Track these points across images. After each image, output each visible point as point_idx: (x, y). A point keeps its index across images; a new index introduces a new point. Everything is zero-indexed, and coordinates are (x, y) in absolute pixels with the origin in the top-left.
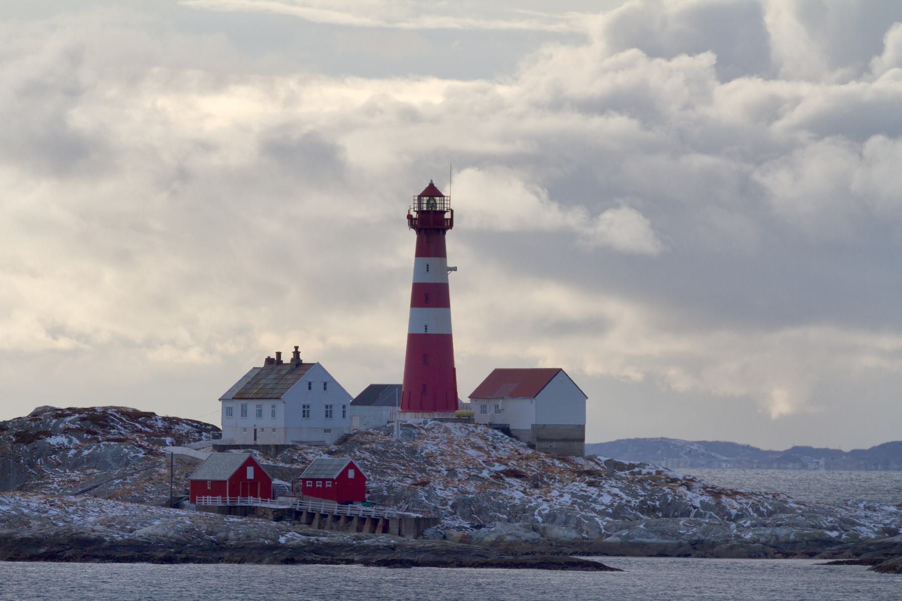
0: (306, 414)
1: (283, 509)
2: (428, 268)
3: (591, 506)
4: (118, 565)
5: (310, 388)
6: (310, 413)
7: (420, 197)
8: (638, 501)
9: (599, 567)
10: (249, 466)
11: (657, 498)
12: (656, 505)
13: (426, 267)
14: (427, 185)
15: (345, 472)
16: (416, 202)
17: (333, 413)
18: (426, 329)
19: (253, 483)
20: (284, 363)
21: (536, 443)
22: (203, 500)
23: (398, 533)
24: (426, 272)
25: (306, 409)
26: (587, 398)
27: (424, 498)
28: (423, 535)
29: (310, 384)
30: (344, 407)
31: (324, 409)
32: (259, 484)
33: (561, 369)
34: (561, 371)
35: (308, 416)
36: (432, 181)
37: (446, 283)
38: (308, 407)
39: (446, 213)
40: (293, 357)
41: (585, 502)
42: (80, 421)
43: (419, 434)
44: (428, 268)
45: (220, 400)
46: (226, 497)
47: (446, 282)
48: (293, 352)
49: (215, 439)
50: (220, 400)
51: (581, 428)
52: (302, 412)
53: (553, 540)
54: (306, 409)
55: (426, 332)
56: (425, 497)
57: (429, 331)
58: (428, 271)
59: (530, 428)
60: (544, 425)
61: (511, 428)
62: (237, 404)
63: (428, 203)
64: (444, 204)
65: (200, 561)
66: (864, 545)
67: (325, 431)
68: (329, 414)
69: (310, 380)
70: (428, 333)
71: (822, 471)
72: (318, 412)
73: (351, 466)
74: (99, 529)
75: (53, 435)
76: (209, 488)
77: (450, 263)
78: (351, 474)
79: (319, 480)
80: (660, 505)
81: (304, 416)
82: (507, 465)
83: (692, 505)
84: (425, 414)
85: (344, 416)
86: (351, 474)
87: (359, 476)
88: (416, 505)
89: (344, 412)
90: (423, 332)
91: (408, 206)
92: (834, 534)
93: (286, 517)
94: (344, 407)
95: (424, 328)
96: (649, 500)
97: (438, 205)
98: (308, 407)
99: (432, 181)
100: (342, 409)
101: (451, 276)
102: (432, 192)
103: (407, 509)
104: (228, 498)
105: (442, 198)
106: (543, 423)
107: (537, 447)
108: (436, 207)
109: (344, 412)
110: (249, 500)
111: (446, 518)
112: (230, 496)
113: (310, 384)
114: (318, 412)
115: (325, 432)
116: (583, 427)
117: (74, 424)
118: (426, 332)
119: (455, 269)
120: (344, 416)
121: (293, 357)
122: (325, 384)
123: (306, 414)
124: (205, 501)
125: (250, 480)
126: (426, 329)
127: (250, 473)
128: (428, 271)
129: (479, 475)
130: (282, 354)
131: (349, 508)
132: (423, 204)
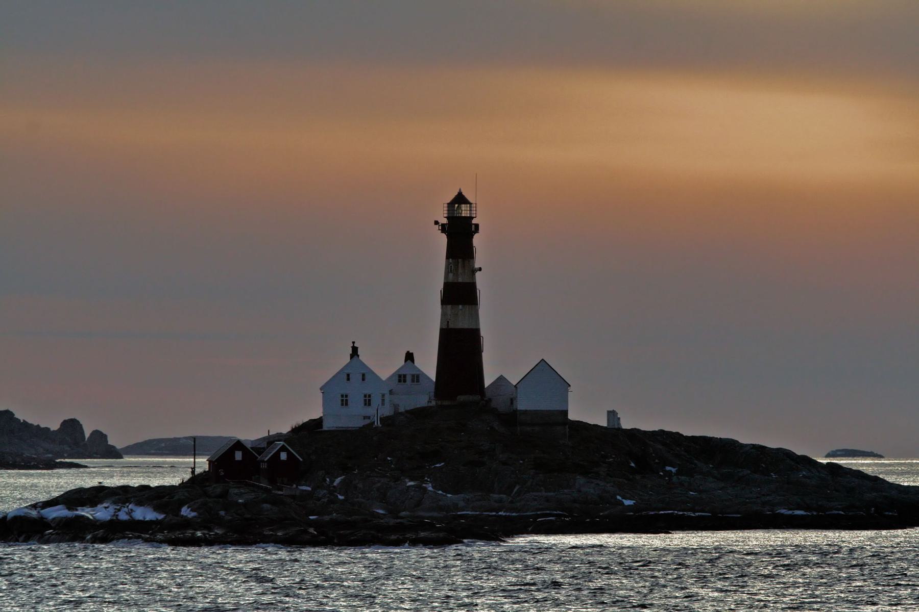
0: (345, 402)
9: (78, 466)
25: (344, 398)
26: (570, 386)
29: (348, 375)
30: (383, 395)
31: (340, 398)
36: (460, 190)
39: (474, 219)
40: (52, 429)
49: (312, 421)
54: (344, 398)
64: (470, 210)
68: (368, 402)
72: (356, 401)
92: (35, 456)
94: (383, 395)
97: (463, 212)
99: (460, 190)
101: (478, 275)
102: (460, 199)
105: (468, 205)
108: (461, 213)
114: (356, 401)
116: (567, 411)
119: (480, 269)
121: (52, 429)
122: (363, 375)
123: (345, 402)
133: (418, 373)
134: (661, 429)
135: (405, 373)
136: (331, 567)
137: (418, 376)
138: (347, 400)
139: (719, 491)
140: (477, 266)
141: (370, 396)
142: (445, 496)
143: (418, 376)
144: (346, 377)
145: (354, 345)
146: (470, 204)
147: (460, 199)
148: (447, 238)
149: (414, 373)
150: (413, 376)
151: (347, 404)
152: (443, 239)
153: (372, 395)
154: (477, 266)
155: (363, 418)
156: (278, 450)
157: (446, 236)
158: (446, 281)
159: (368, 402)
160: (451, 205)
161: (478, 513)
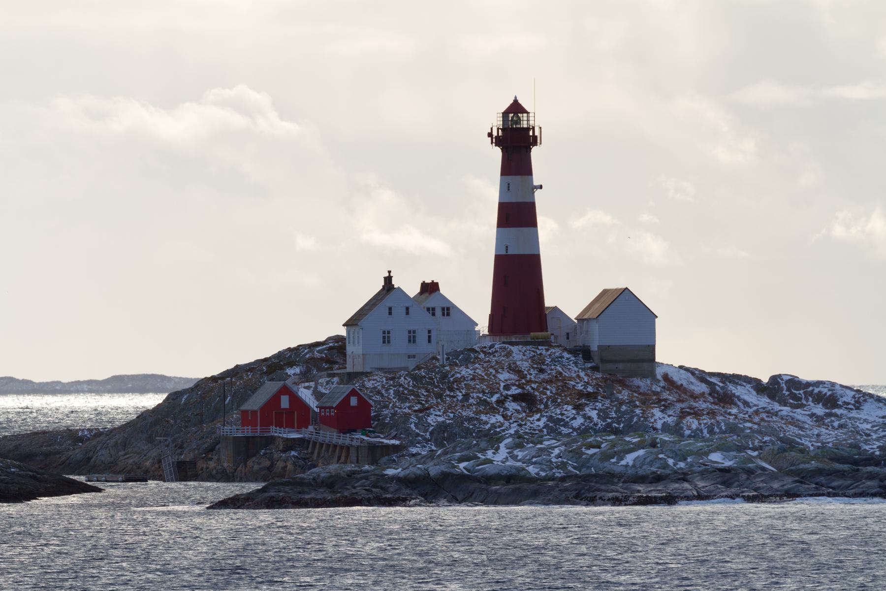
0: (386, 339)
1: (294, 439)
2: (509, 187)
3: (559, 430)
4: (384, 510)
8: (604, 424)
10: (289, 397)
11: (623, 419)
12: (619, 427)
14: (512, 102)
17: (417, 338)
18: (507, 250)
19: (289, 412)
20: (395, 287)
21: (600, 365)
22: (246, 431)
23: (356, 461)
24: (507, 190)
25: (386, 335)
26: (657, 317)
27: (412, 426)
28: (377, 463)
29: (390, 309)
31: (382, 335)
32: (296, 413)
33: (627, 288)
34: (627, 290)
35: (389, 342)
36: (516, 97)
37: (530, 203)
38: (389, 332)
41: (555, 426)
42: (328, 350)
43: (477, 358)
44: (509, 187)
45: (344, 325)
46: (257, 426)
47: (532, 201)
48: (385, 278)
50: (344, 325)
51: (652, 349)
52: (427, 337)
53: (219, 456)
55: (507, 252)
56: (415, 423)
58: (509, 190)
59: (596, 349)
60: (609, 346)
61: (592, 349)
65: (369, 503)
67: (409, 357)
69: (390, 305)
70: (509, 253)
73: (354, 393)
74: (869, 487)
75: (295, 365)
77: (536, 180)
78: (354, 401)
80: (623, 427)
81: (384, 342)
82: (523, 388)
83: (652, 427)
84: (502, 337)
85: (429, 341)
86: (354, 401)
87: (363, 403)
88: (403, 432)
89: (429, 337)
90: (504, 253)
91: (496, 122)
93: (297, 446)
95: (504, 248)
96: (615, 423)
98: (389, 332)
99: (516, 97)
100: (427, 335)
101: (538, 194)
102: (516, 108)
103: (395, 436)
104: (259, 427)
106: (608, 344)
107: (601, 369)
109: (429, 337)
110: (271, 430)
111: (417, 445)
112: (260, 427)
115: (409, 358)
117: (321, 353)
118: (507, 252)
119: (541, 187)
120: (429, 341)
123: (386, 339)
124: (247, 432)
126: (507, 250)
128: (509, 190)
129: (488, 399)
130: (393, 278)
131: (328, 436)
132: (523, 120)
133: (448, 306)
134: (112, 375)
135: (433, 306)
136: (514, 560)
137: (448, 309)
138: (389, 337)
139: (227, 402)
140: (536, 182)
141: (414, 332)
142: (858, 470)
143: (448, 309)
144: (404, 311)
145: (390, 274)
146: (528, 113)
147: (516, 108)
148: (502, 152)
149: (445, 306)
150: (443, 309)
151: (414, 342)
152: (497, 152)
153: (432, 331)
154: (536, 182)
155: (407, 357)
156: (347, 395)
157: (500, 151)
158: (508, 199)
159: (412, 338)
160: (505, 114)
161: (393, 442)
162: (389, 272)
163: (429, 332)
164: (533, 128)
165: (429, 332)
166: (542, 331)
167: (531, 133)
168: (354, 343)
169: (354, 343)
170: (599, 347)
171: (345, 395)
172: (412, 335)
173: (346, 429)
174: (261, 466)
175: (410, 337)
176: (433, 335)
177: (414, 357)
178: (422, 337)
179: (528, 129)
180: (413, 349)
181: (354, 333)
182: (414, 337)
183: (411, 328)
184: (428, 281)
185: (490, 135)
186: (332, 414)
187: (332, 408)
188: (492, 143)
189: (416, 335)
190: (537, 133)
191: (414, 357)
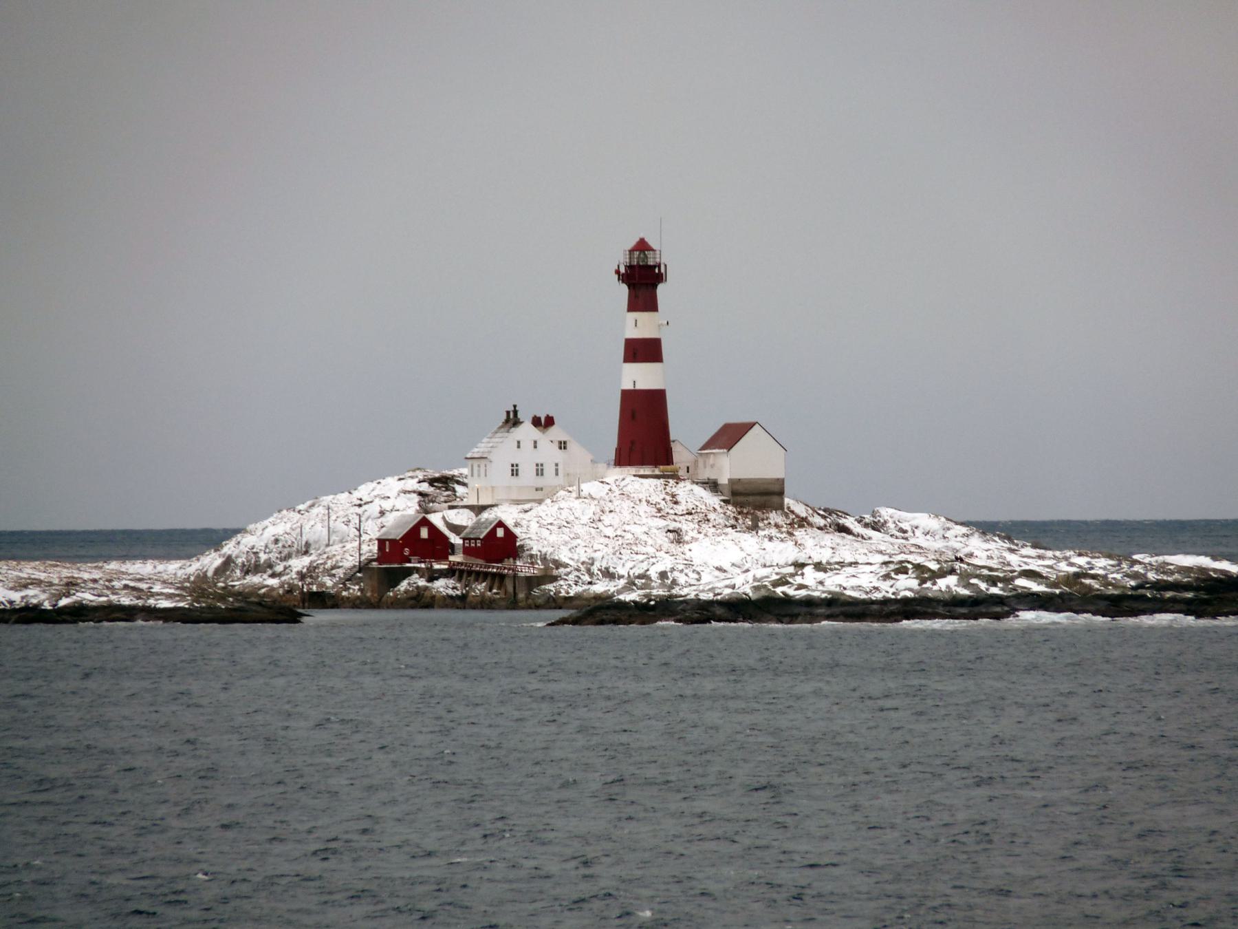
0: (515, 472)
5: (519, 447)
6: (544, 472)
7: (631, 251)
13: (634, 322)
15: (493, 531)
16: (628, 256)
29: (519, 442)
31: (535, 467)
34: (757, 425)
35: (517, 475)
57: (639, 387)
59: (726, 482)
62: (479, 466)
63: (639, 258)
66: (777, 612)
67: (537, 490)
69: (518, 439)
71: (260, 545)
76: (387, 550)
78: (500, 533)
79: (473, 539)
85: (557, 474)
86: (500, 533)
89: (557, 470)
90: (632, 388)
100: (554, 468)
109: (557, 470)
113: (519, 442)
120: (557, 474)
123: (515, 472)
125: (500, 538)
127: (424, 533)
144: (532, 445)
152: (624, 290)
159: (540, 471)
162: (515, 406)
163: (557, 465)
164: (659, 266)
165: (557, 465)
166: (668, 464)
167: (657, 271)
168: (479, 475)
169: (479, 475)
170: (730, 480)
171: (493, 525)
172: (540, 467)
173: (490, 559)
174: (906, 608)
175: (537, 470)
176: (560, 467)
177: (542, 489)
178: (549, 470)
179: (654, 267)
180: (540, 482)
181: (479, 466)
182: (542, 470)
183: (539, 462)
184: (538, 416)
185: (618, 272)
186: (479, 545)
187: (479, 539)
188: (619, 279)
189: (544, 467)
190: (663, 270)
191: (542, 489)
